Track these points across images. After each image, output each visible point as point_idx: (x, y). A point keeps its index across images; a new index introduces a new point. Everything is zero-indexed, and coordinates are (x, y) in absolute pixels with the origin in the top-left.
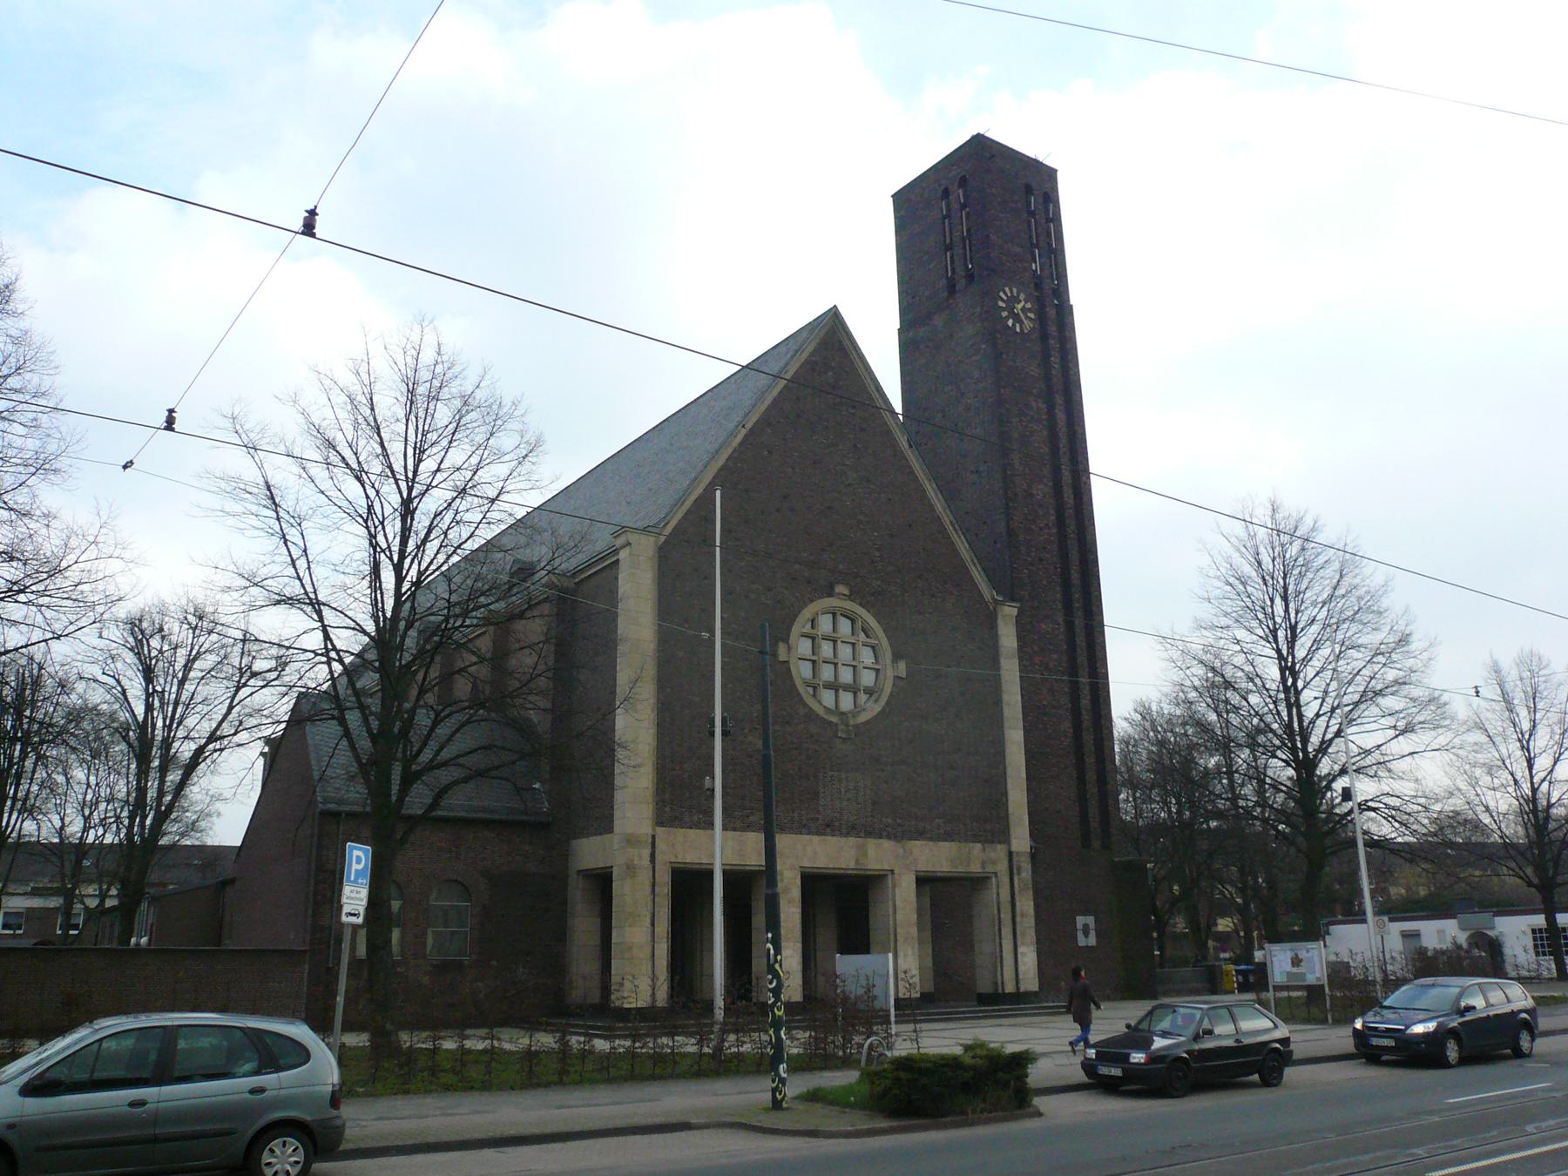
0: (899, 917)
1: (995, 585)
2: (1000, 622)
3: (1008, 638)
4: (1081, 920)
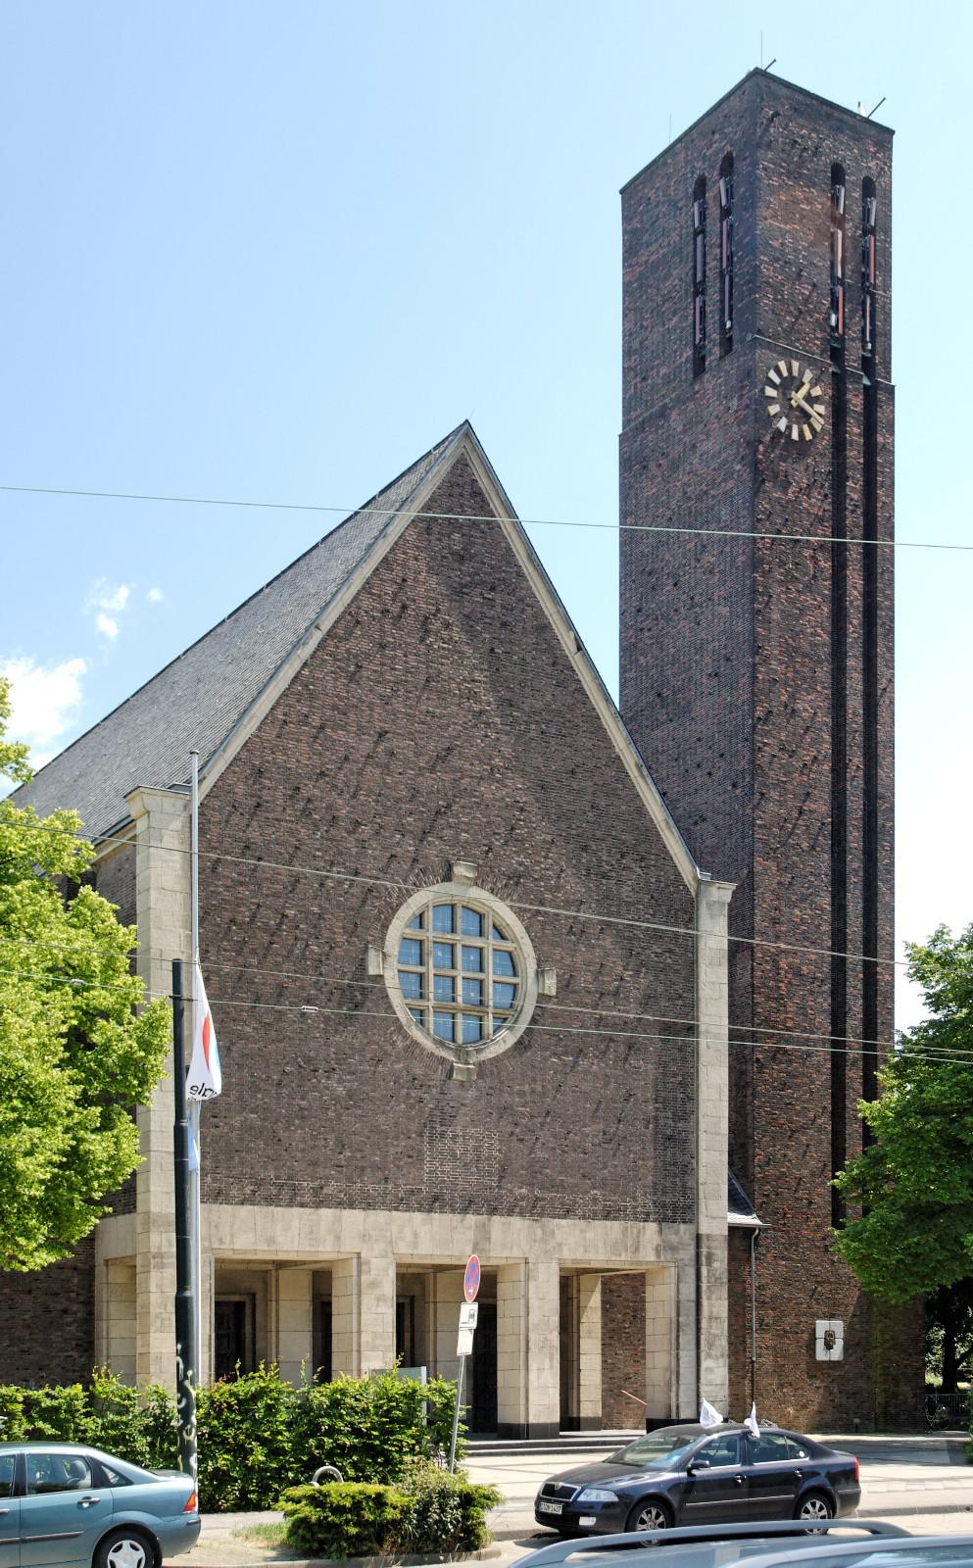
0: (364, 1338)
1: (697, 857)
2: (703, 912)
3: (714, 936)
4: (822, 1326)
